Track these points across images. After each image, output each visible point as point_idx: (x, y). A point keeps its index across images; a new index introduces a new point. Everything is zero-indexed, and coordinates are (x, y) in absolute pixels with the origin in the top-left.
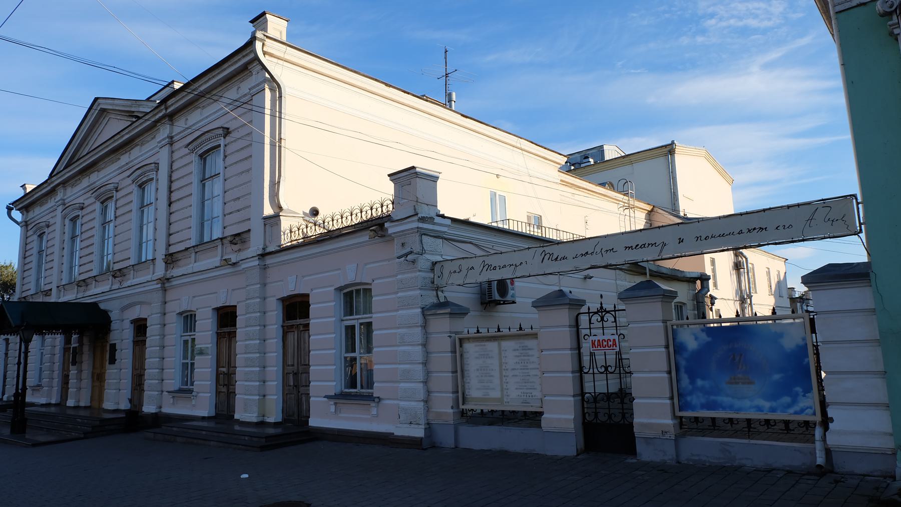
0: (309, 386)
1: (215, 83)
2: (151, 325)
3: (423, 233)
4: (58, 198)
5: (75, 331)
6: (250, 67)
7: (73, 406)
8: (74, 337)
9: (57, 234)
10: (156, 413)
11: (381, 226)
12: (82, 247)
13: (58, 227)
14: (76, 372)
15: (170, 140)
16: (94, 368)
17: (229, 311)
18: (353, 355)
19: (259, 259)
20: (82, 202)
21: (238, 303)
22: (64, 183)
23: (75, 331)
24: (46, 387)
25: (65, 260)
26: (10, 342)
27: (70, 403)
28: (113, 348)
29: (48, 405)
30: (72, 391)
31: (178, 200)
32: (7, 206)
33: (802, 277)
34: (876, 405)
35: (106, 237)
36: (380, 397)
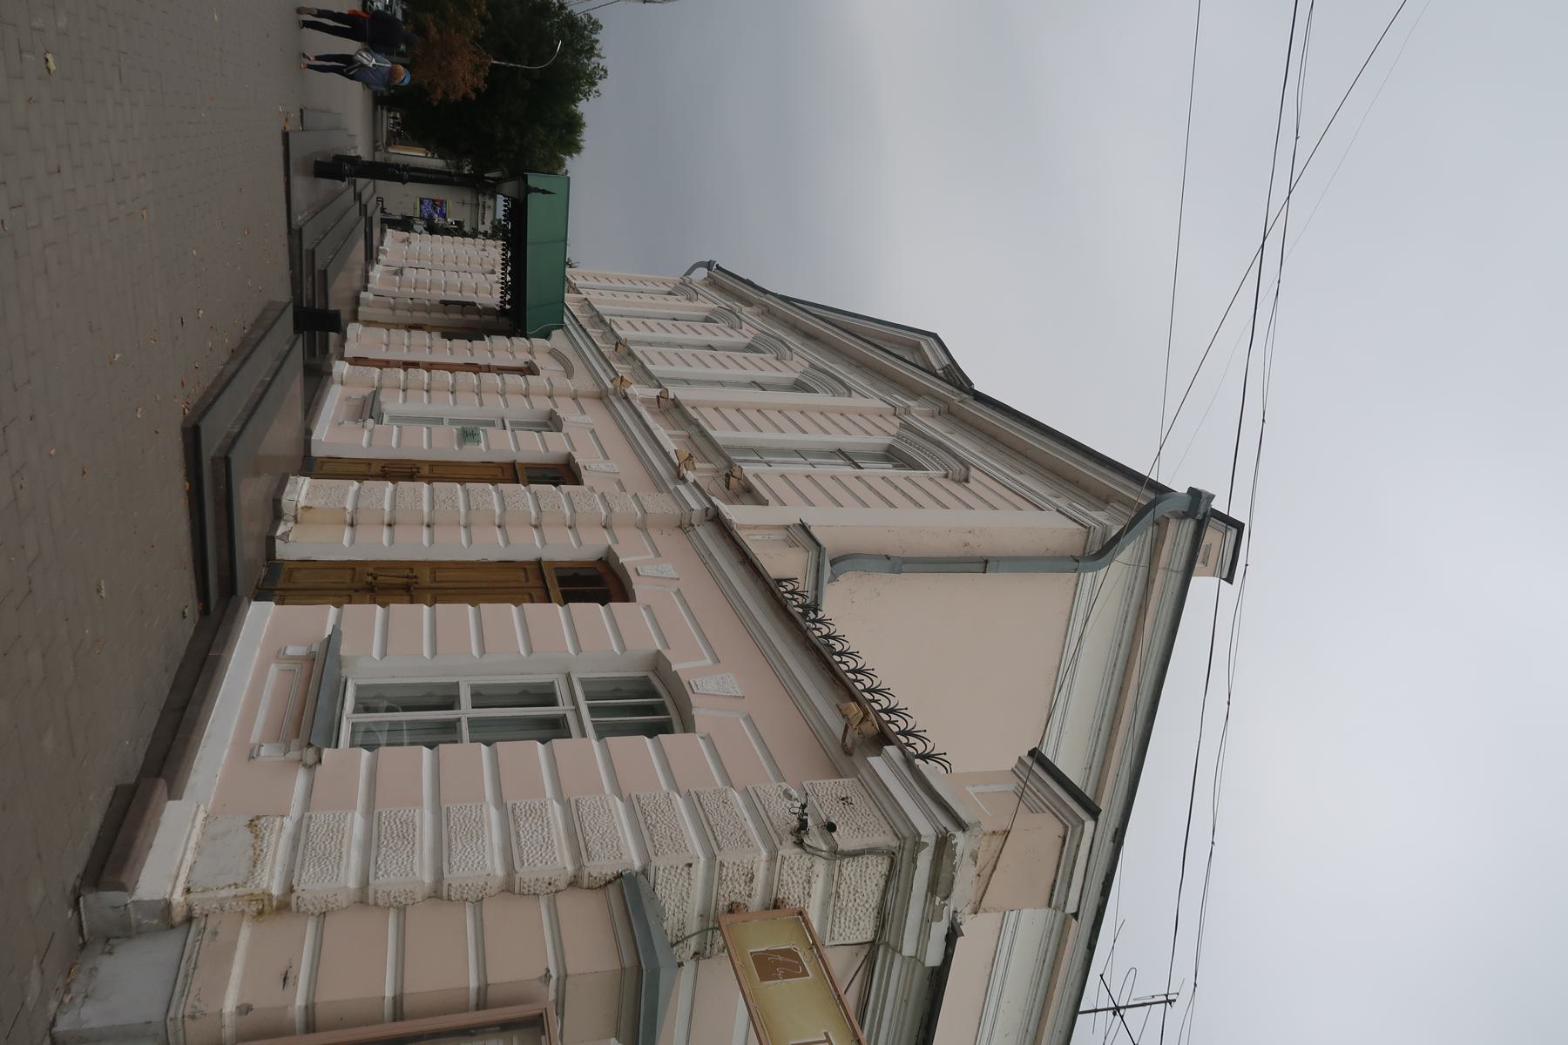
0: (375, 603)
3: (897, 865)
5: (509, 302)
6: (1115, 505)
10: (331, 374)
11: (882, 739)
17: (559, 589)
18: (464, 726)
19: (707, 509)
23: (509, 302)
33: (180, 799)
34: (537, 587)
36: (319, 768)
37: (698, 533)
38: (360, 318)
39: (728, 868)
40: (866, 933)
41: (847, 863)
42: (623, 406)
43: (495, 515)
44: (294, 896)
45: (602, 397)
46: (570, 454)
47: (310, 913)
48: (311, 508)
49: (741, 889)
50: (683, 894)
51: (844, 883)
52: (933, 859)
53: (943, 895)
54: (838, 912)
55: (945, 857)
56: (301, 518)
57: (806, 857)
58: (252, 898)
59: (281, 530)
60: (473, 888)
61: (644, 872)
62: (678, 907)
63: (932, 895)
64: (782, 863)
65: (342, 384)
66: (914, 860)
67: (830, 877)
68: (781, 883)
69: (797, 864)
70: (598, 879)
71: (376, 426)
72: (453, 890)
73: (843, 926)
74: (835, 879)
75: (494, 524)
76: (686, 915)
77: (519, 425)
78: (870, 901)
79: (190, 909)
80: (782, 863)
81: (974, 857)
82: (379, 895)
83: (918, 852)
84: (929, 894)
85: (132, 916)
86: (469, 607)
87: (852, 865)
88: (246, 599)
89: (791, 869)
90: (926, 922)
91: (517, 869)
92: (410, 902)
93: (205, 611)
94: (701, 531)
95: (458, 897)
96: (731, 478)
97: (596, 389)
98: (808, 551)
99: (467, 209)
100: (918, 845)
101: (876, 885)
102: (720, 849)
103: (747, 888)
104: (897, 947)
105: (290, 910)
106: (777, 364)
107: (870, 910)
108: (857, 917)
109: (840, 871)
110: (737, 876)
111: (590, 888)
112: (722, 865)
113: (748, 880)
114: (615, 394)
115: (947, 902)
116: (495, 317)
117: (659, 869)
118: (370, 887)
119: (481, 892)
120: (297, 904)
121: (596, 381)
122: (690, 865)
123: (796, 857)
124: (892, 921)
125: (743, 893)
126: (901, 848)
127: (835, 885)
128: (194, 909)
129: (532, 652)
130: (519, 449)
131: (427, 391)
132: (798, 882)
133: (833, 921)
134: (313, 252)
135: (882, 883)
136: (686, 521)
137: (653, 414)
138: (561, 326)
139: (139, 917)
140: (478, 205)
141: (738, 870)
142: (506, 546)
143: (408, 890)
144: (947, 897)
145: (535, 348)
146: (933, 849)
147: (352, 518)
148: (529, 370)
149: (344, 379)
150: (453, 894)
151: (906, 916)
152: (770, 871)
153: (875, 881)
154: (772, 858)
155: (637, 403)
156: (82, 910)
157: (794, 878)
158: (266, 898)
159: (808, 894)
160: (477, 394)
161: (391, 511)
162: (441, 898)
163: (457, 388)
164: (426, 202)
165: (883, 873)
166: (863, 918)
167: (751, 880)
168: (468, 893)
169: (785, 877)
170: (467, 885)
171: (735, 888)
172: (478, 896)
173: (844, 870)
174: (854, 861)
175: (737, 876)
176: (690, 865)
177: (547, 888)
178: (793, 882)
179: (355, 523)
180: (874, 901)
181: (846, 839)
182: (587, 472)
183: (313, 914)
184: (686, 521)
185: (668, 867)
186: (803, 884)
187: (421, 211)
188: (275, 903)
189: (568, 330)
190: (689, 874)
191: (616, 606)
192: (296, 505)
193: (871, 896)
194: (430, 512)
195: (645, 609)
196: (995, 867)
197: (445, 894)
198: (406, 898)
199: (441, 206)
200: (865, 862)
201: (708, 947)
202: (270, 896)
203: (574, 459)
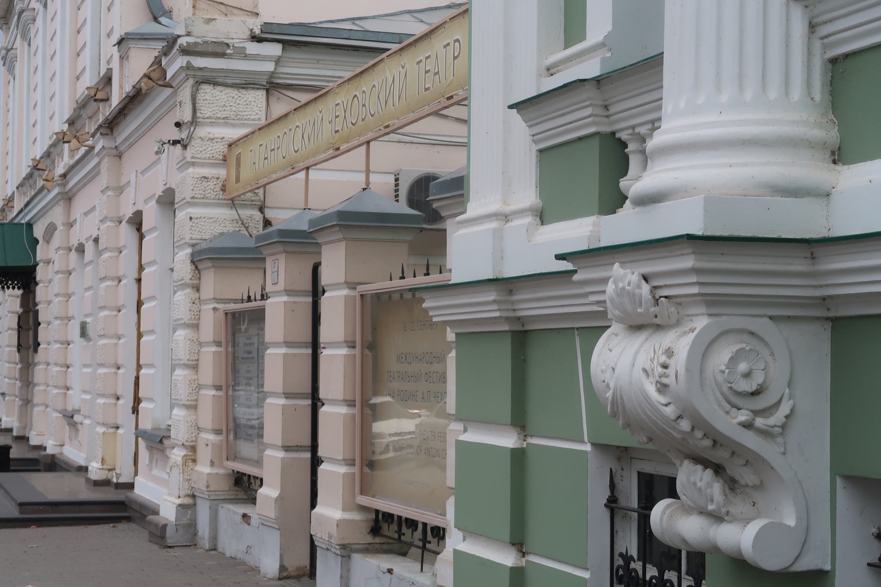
19: (101, 134)
37: (120, 143)
39: (196, 194)
40: (258, 96)
41: (201, 113)
42: (71, 178)
43: (110, 315)
44: (186, 443)
45: (68, 198)
47: (197, 435)
48: (103, 459)
49: (212, 184)
50: (211, 221)
51: (217, 115)
52: (199, 56)
53: (226, 47)
54: (239, 117)
55: (196, 50)
56: (110, 465)
57: (193, 143)
58: (185, 463)
59: (115, 480)
60: (191, 347)
61: (193, 246)
62: (221, 224)
63: (226, 55)
64: (196, 158)
65: (62, 446)
66: (200, 69)
67: (212, 124)
68: (211, 158)
69: (198, 148)
70: (194, 275)
71: (81, 413)
72: (191, 358)
73: (250, 113)
74: (213, 121)
75: (117, 315)
76: (227, 219)
78: (232, 95)
79: (188, 496)
80: (196, 158)
81: (209, 21)
82: (190, 399)
83: (195, 68)
84: (225, 57)
85: (183, 522)
87: (204, 110)
88: (129, 494)
89: (201, 152)
90: (246, 57)
91: (183, 322)
92: (197, 382)
93: (128, 519)
94: (119, 140)
95: (196, 355)
97: (61, 203)
98: (130, 48)
100: (189, 67)
101: (221, 92)
102: (184, 199)
103: (211, 181)
104: (268, 74)
105: (195, 445)
107: (239, 94)
108: (244, 103)
109: (207, 118)
110: (202, 188)
111: (200, 279)
112: (193, 198)
113: (206, 180)
114: (64, 185)
115: (231, 45)
117: (192, 237)
118: (186, 404)
119: (195, 342)
120: (191, 442)
122: (191, 218)
123: (193, 150)
124: (250, 78)
125: (215, 183)
126: (194, 76)
127: (218, 121)
128: (187, 494)
129: (154, 296)
130: (91, 287)
131: (68, 367)
132: (212, 146)
133: (246, 119)
134: (21, 505)
135: (219, 88)
136: (114, 152)
139: (185, 519)
141: (198, 187)
142: (126, 307)
143: (188, 383)
144: (228, 45)
145: (43, 258)
146: (192, 57)
147: (112, 427)
149: (58, 444)
150: (194, 358)
151: (244, 71)
152: (203, 165)
153: (217, 93)
154: (193, 164)
155: (72, 162)
156: (174, 545)
157: (209, 149)
158: (185, 458)
159: (222, 139)
160: (70, 321)
161: (106, 397)
162: (197, 365)
163: (64, 339)
165: (212, 88)
166: (246, 99)
167: (205, 178)
168: (195, 350)
169: (207, 155)
170: (189, 350)
171: (210, 188)
172: (197, 344)
173: (207, 116)
174: (200, 109)
175: (202, 188)
176: (191, 218)
177: (196, 305)
178: (211, 150)
179: (115, 425)
180: (233, 92)
181: (186, 115)
183: (198, 434)
184: (114, 152)
185: (191, 231)
186: (214, 143)
188: (190, 454)
190: (197, 219)
192: (100, 469)
193: (230, 95)
194: (107, 367)
195: (147, 204)
196: (221, 3)
197: (194, 363)
198: (194, 384)
200: (202, 102)
201: (254, 203)
202: (184, 456)
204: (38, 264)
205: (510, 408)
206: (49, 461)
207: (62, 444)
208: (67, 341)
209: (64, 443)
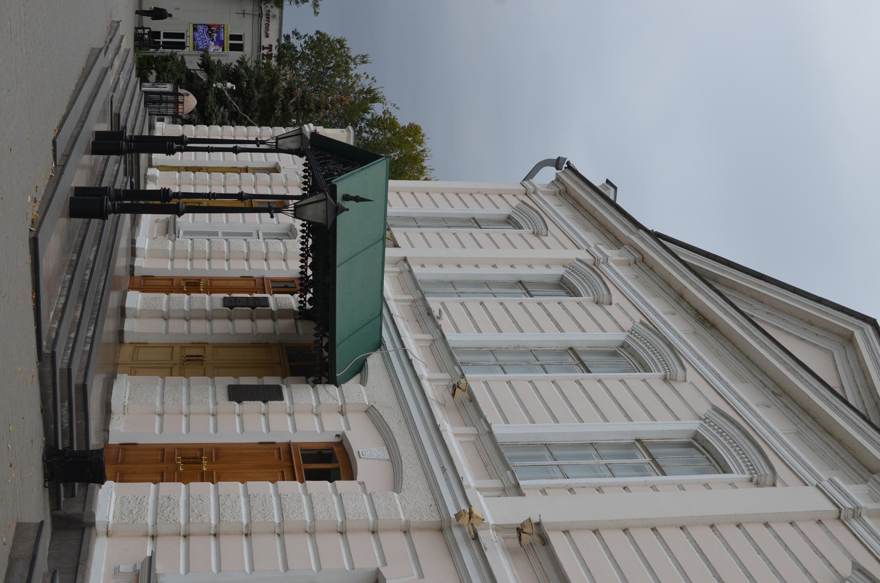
0: (180, 482)
1: (712, 310)
2: (340, 497)
4: (608, 252)
7: (127, 305)
8: (292, 301)
9: (523, 252)
10: (93, 524)
12: (558, 382)
13: (540, 252)
14: (208, 309)
15: (532, 191)
16: (216, 346)
20: (614, 301)
21: (362, 484)
22: (642, 263)
24: (174, 246)
25: (468, 271)
26: (273, 174)
27: (135, 299)
28: (274, 394)
29: (133, 253)
30: (162, 300)
31: (447, 200)
32: (565, 159)
35: (494, 290)
38: (154, 164)
46: (378, 572)
77: (268, 236)
86: (240, 484)
96: (457, 389)
99: (248, 20)
106: (533, 240)
116: (292, 321)
121: (435, 500)
137: (510, 552)
138: (379, 345)
140: (260, 16)
148: (276, 169)
149: (110, 529)
164: (200, 29)
182: (360, 459)
187: (194, 40)
189: (388, 354)
191: (342, 485)
199: (218, 33)
203: (294, 226)
204: (338, 387)
205: (136, 261)
206: (86, 520)
207: (110, 533)
208: (229, 259)
209: (111, 536)
